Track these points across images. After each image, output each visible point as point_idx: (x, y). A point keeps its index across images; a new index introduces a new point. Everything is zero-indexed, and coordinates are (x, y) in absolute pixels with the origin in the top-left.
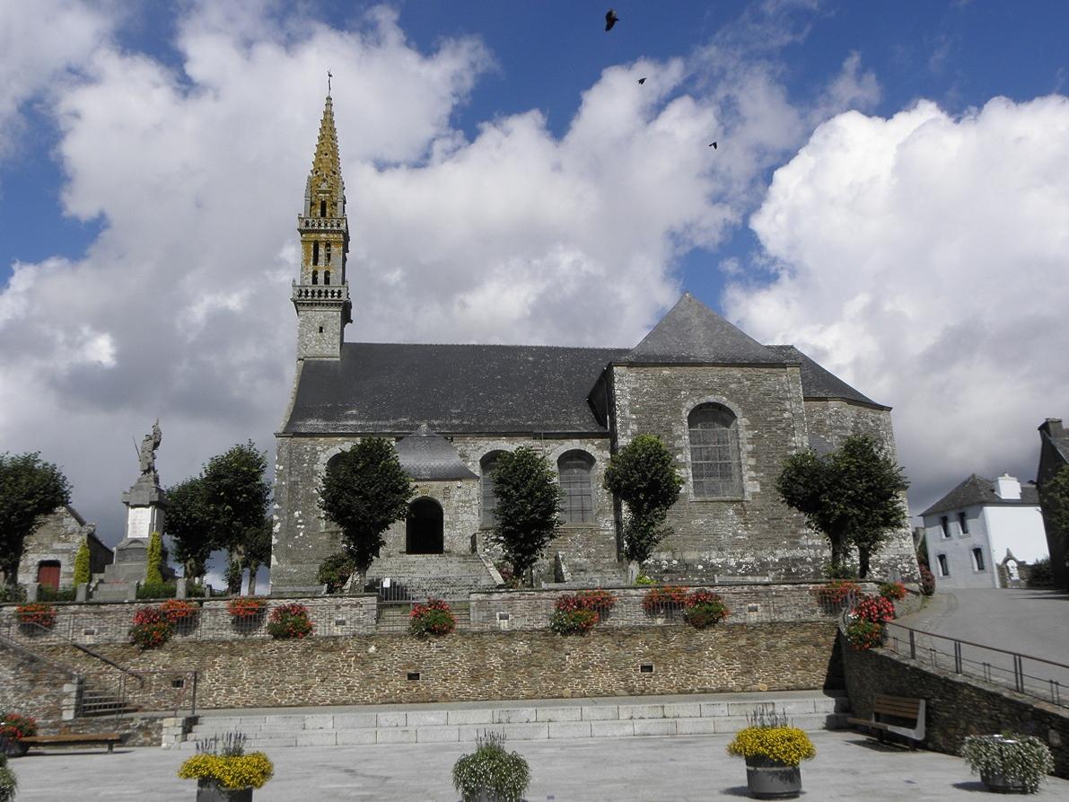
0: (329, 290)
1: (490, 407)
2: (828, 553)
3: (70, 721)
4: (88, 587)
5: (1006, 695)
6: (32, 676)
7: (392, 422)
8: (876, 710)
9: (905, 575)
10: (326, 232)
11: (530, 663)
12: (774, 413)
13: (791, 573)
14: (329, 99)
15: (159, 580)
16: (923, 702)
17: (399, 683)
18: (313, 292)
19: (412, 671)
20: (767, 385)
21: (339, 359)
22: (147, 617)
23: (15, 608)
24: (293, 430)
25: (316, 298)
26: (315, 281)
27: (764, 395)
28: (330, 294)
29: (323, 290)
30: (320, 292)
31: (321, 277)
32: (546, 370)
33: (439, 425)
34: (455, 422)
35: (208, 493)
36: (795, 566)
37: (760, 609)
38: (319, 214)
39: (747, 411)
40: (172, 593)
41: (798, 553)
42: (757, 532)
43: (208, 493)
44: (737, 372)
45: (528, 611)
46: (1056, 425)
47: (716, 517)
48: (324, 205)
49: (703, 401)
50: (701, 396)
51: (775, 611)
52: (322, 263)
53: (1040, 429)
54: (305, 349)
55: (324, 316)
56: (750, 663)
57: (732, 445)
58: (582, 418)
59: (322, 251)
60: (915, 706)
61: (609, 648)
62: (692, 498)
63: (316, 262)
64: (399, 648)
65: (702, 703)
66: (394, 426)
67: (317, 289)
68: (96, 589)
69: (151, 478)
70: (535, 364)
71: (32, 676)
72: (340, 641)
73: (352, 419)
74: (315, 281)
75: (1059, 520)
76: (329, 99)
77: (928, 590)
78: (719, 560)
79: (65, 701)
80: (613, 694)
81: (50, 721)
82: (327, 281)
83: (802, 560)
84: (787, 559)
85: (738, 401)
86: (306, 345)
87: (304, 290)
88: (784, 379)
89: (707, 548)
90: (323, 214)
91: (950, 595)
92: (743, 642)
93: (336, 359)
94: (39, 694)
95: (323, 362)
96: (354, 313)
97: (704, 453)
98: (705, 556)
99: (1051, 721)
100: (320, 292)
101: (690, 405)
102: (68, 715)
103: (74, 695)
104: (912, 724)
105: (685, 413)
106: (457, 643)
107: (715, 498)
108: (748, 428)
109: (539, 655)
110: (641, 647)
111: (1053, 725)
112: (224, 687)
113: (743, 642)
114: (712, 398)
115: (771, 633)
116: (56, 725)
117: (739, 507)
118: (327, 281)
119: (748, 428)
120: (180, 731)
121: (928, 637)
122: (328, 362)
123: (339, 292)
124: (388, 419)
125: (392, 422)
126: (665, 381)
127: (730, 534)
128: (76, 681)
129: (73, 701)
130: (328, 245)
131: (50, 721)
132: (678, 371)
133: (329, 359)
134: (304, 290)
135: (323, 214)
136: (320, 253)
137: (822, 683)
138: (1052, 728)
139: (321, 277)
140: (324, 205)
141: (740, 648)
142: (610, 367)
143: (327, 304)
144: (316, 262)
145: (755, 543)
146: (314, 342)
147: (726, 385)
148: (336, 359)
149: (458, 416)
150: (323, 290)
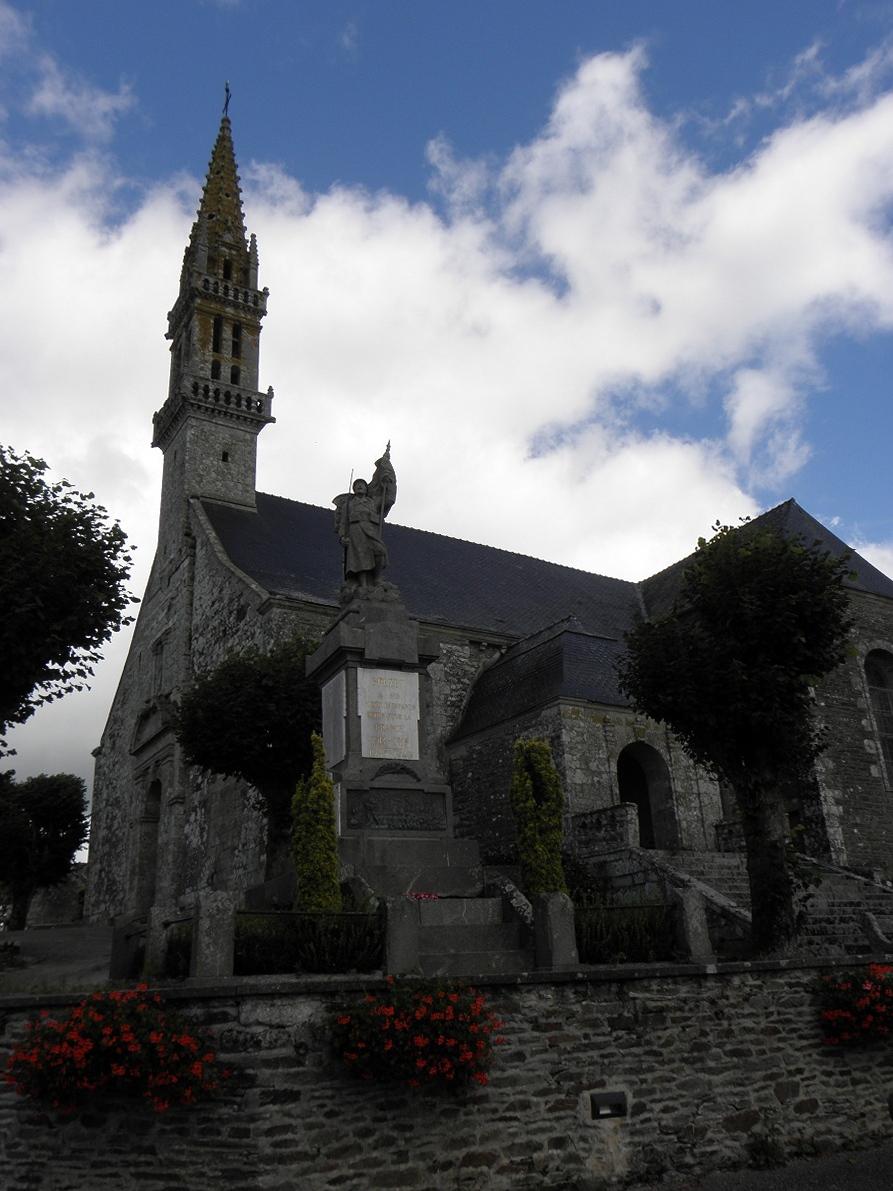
0: (234, 393)
14: (226, 121)
21: (255, 511)
23: (572, 1083)
25: (232, 406)
28: (244, 402)
31: (226, 372)
52: (227, 352)
54: (199, 483)
55: (231, 436)
59: (227, 333)
63: (217, 348)
73: (862, 876)
75: (584, 1149)
76: (226, 121)
86: (200, 476)
93: (250, 510)
95: (229, 508)
122: (238, 510)
133: (239, 507)
136: (225, 336)
139: (226, 372)
143: (238, 417)
144: (217, 348)
146: (214, 475)
148: (250, 510)
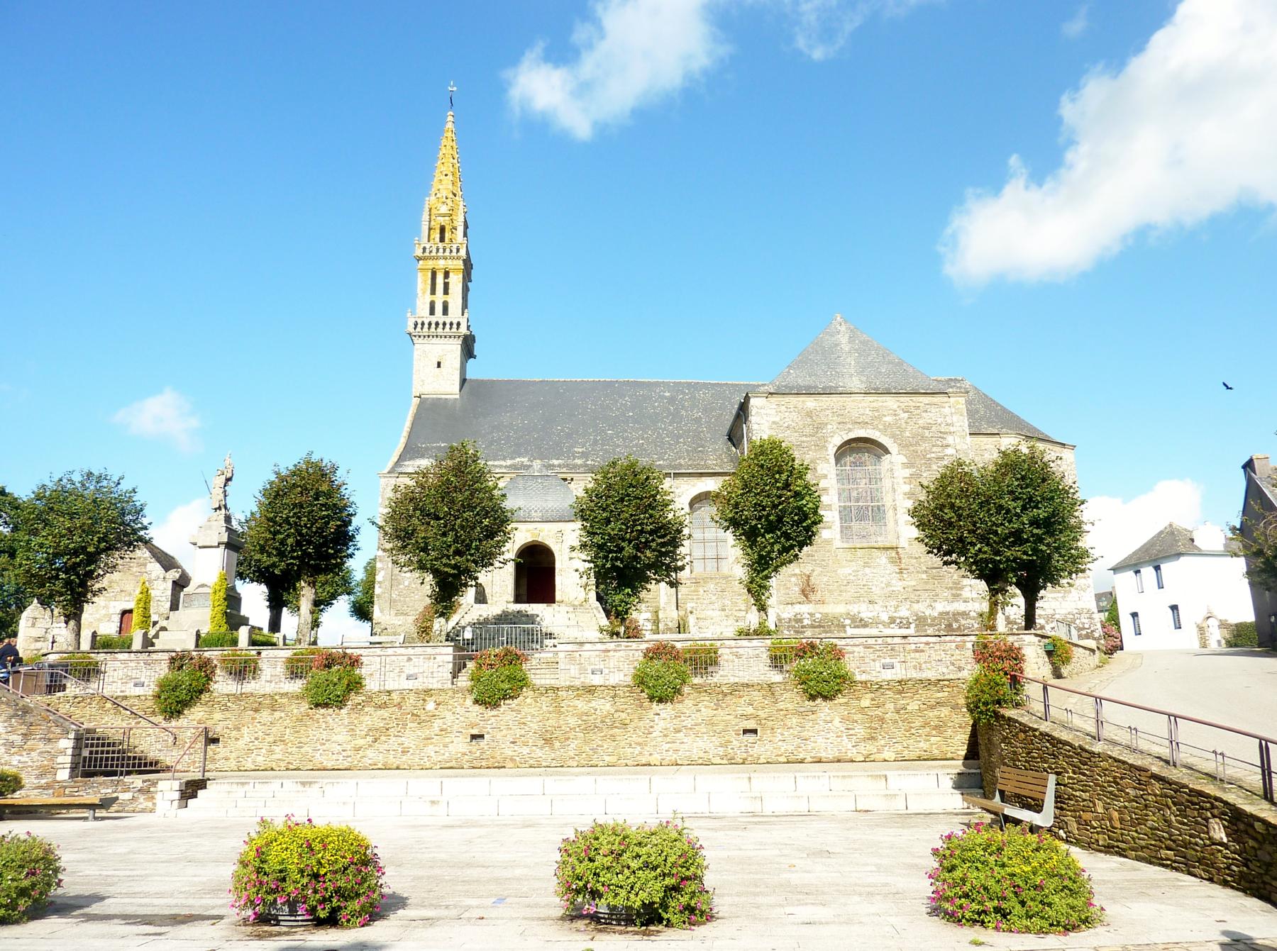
0: (448, 322)
1: (618, 446)
2: (985, 607)
3: (64, 781)
4: (145, 634)
5: (1154, 769)
6: (23, 729)
7: (509, 462)
8: (999, 786)
9: (1084, 632)
10: (445, 258)
11: (614, 724)
12: (934, 449)
13: (950, 626)
15: (225, 628)
16: (1052, 779)
17: (460, 745)
18: (430, 324)
19: (475, 732)
20: (927, 418)
22: (464, 651)
24: (400, 470)
26: (432, 312)
27: (924, 428)
29: (441, 322)
30: (437, 324)
31: (439, 308)
32: (683, 407)
33: (559, 466)
34: (579, 462)
35: (1076, 514)
36: (957, 621)
37: (897, 665)
38: (438, 239)
39: (904, 446)
40: (235, 642)
41: (960, 607)
42: (914, 583)
43: (1076, 514)
44: (891, 402)
45: (622, 662)
46: (1264, 462)
47: (866, 565)
48: (442, 230)
49: (852, 435)
50: (850, 430)
51: (915, 667)
53: (1244, 467)
56: (876, 728)
57: (887, 483)
58: (719, 457)
60: (1040, 789)
61: (706, 708)
62: (838, 543)
64: (461, 705)
65: (798, 775)
66: (510, 466)
67: (433, 319)
68: (156, 636)
69: (222, 517)
70: (672, 400)
71: (23, 729)
72: (394, 696)
74: (432, 312)
77: (1113, 647)
78: (870, 615)
79: (60, 759)
80: (709, 763)
81: (43, 781)
82: (445, 311)
83: (965, 614)
84: (948, 613)
85: (893, 436)
87: (420, 322)
88: (947, 410)
89: (857, 599)
90: (442, 239)
91: (1139, 655)
92: (866, 702)
94: (32, 750)
96: (477, 349)
97: (854, 494)
98: (854, 609)
99: (1213, 807)
100: (437, 324)
101: (838, 441)
102: (63, 775)
103: (70, 752)
104: (1037, 807)
105: (832, 450)
106: (528, 701)
107: (865, 545)
108: (905, 466)
109: (623, 715)
110: (741, 706)
111: (1216, 812)
112: (265, 746)
113: (866, 702)
114: (862, 433)
115: (900, 693)
116: (48, 787)
117: (894, 554)
118: (445, 311)
119: (905, 466)
120: (177, 795)
121: (1060, 705)
123: (459, 324)
124: (504, 459)
125: (509, 462)
126: (809, 414)
127: (875, 578)
128: (72, 736)
129: (69, 759)
130: (447, 275)
131: (43, 781)
132: (825, 401)
134: (420, 322)
135: (442, 239)
137: (964, 753)
138: (1214, 816)
139: (439, 308)
140: (442, 230)
141: (863, 710)
142: (747, 398)
145: (913, 595)
147: (879, 418)
149: (584, 455)
150: (441, 322)
